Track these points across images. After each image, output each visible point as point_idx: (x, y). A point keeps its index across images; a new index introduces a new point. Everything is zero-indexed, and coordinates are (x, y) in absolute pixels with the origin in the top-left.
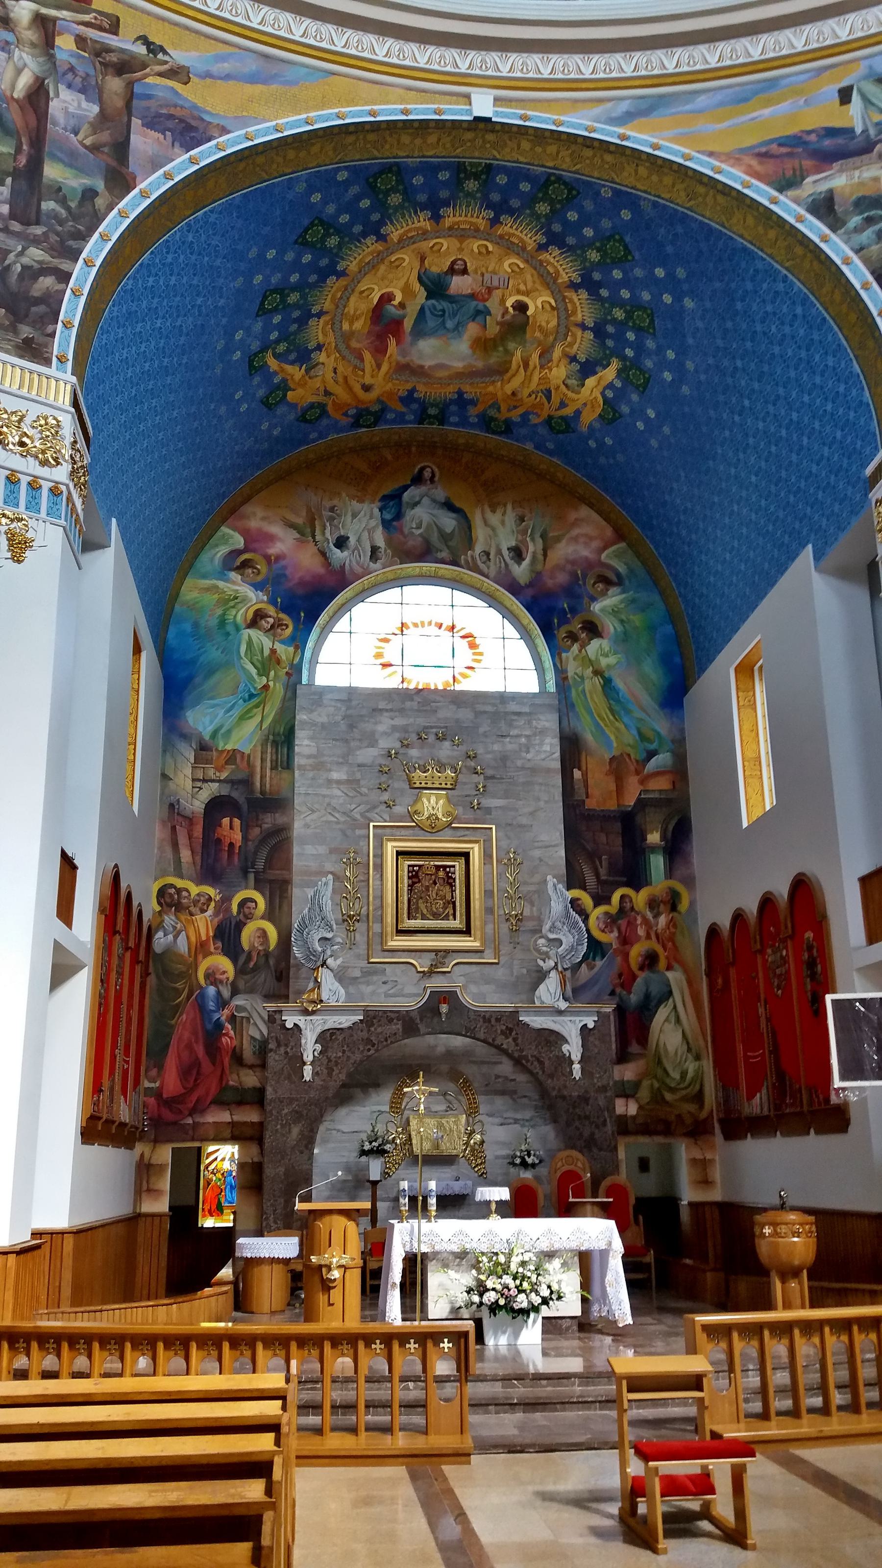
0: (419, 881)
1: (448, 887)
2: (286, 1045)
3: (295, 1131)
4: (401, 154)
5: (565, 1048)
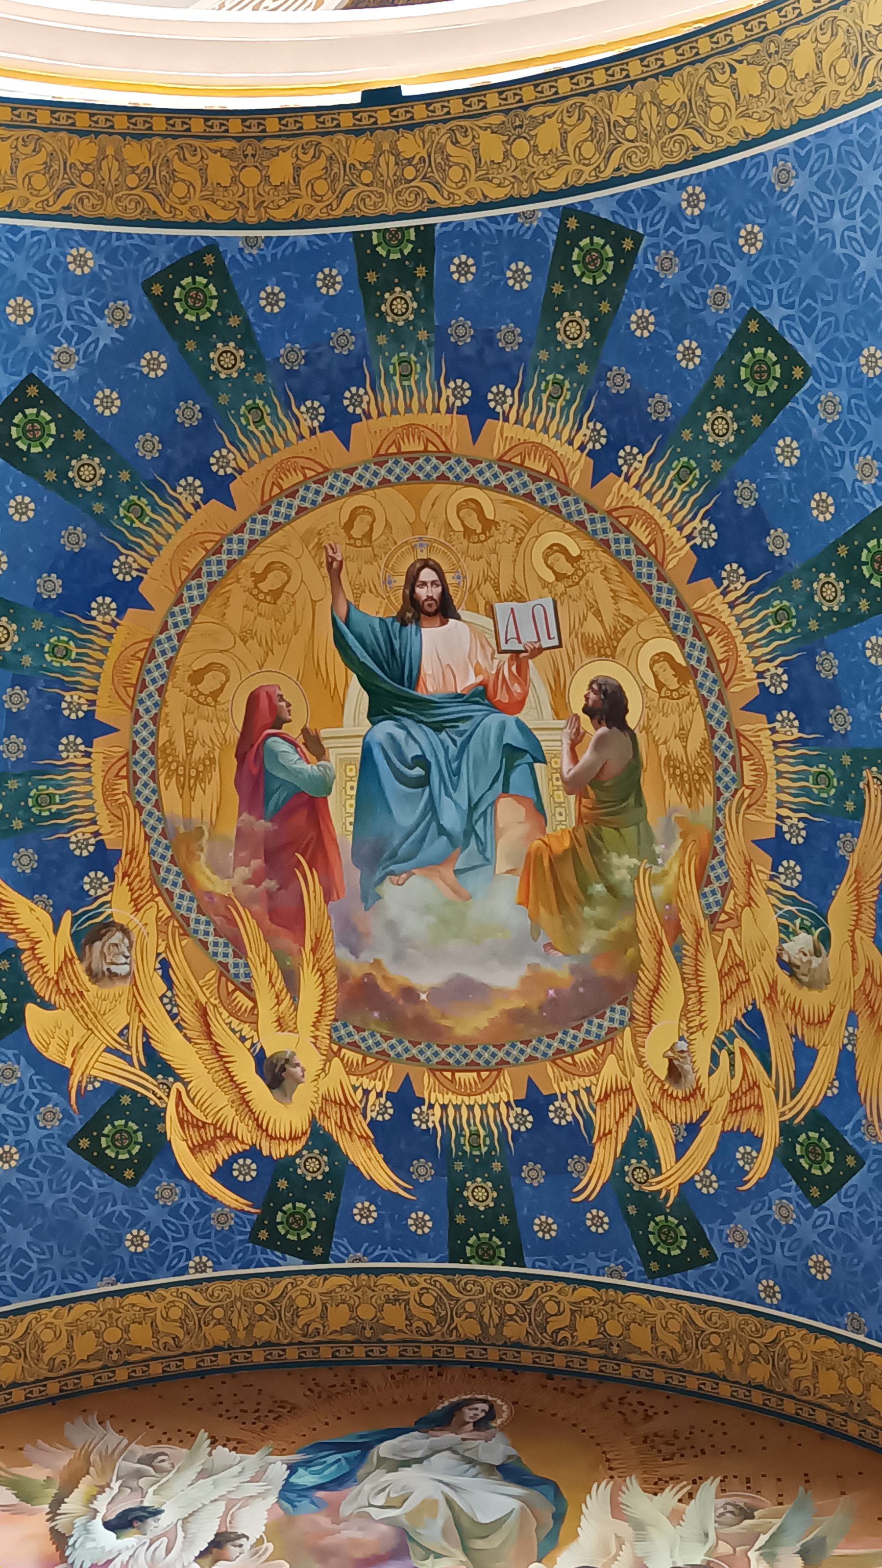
4: (138, 1299)
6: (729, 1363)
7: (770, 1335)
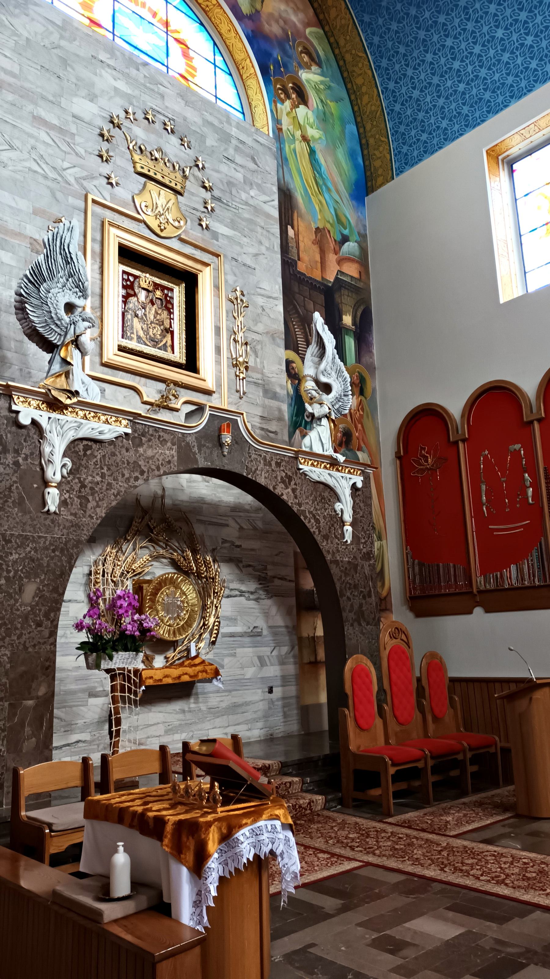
0: (135, 295)
1: (166, 312)
2: (17, 452)
3: (30, 589)
5: (338, 506)
6: (370, 131)
7: (383, 139)
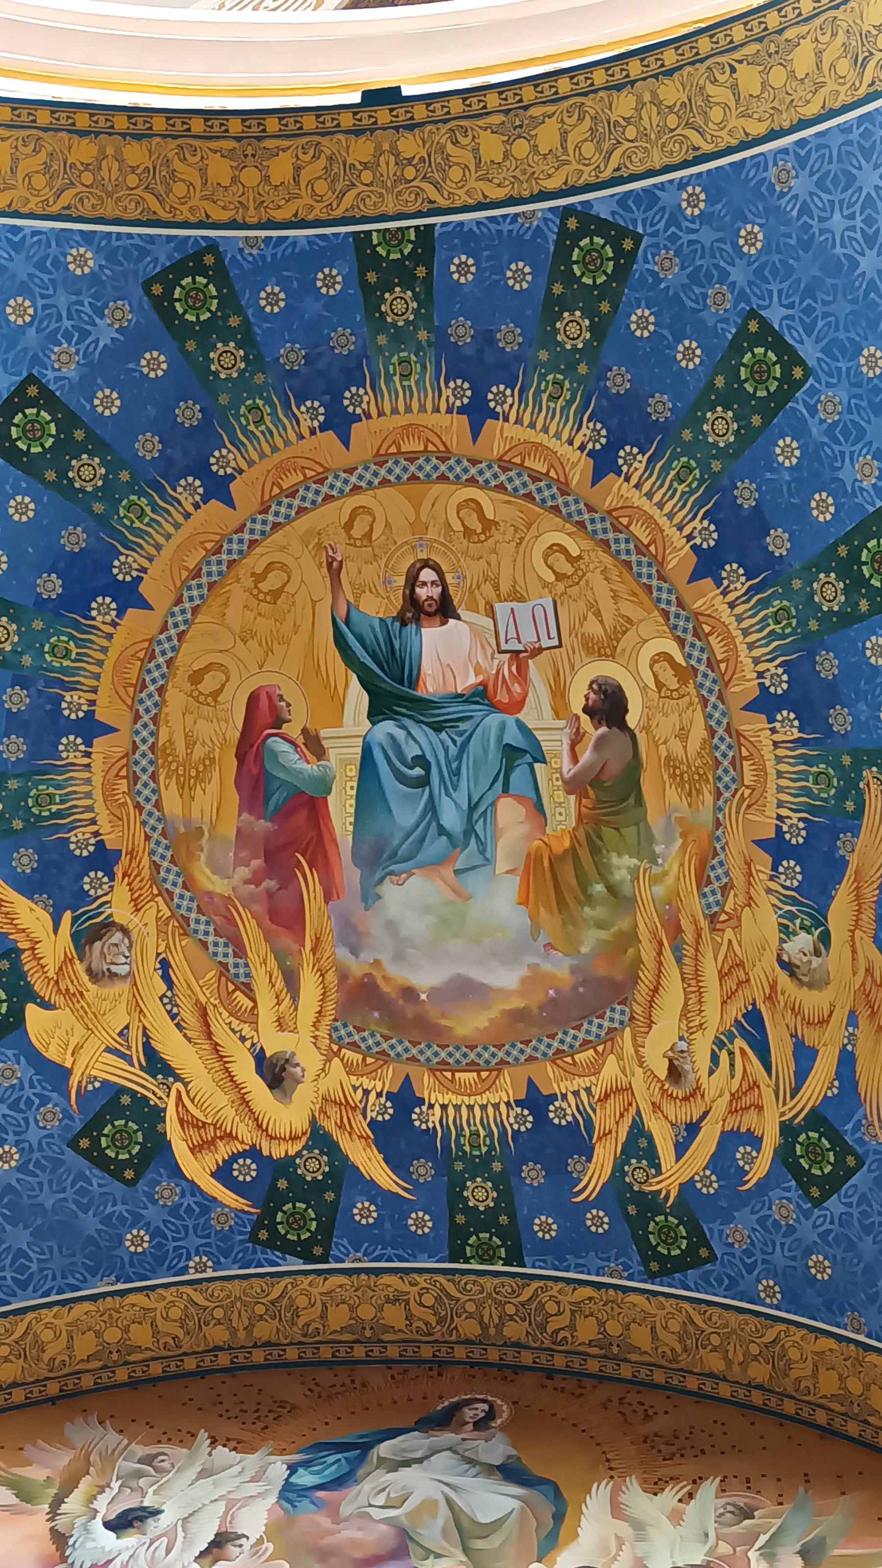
6: (729, 1363)
7: (770, 1335)
